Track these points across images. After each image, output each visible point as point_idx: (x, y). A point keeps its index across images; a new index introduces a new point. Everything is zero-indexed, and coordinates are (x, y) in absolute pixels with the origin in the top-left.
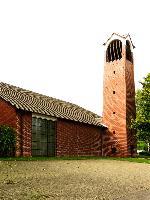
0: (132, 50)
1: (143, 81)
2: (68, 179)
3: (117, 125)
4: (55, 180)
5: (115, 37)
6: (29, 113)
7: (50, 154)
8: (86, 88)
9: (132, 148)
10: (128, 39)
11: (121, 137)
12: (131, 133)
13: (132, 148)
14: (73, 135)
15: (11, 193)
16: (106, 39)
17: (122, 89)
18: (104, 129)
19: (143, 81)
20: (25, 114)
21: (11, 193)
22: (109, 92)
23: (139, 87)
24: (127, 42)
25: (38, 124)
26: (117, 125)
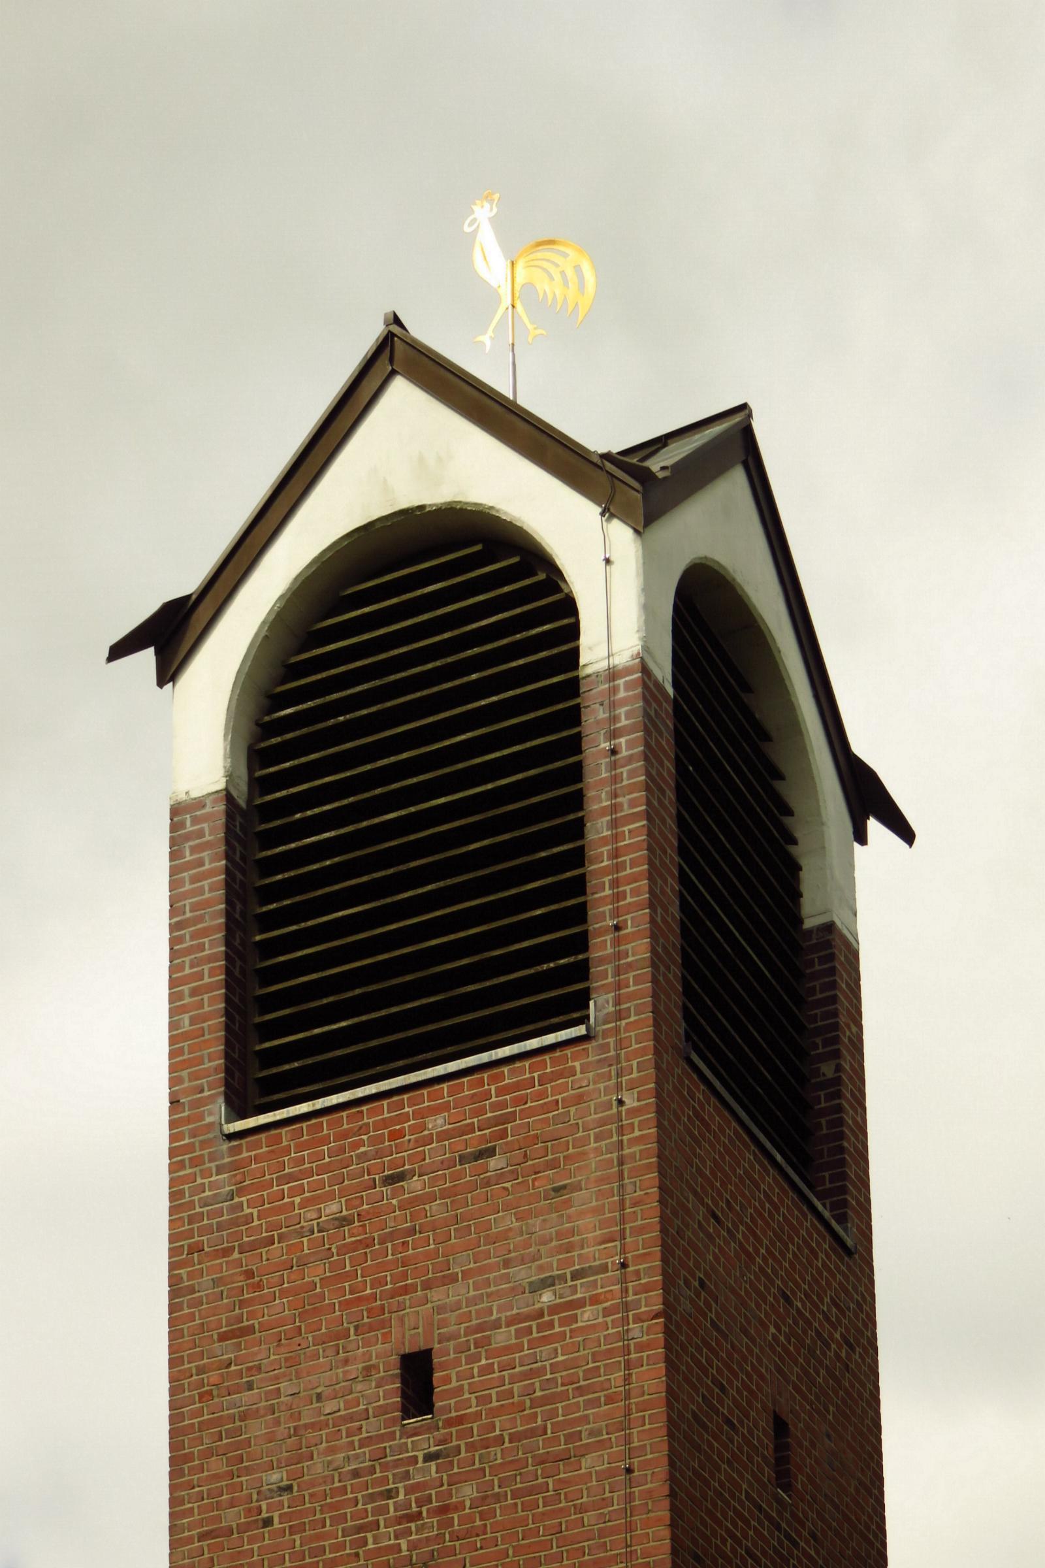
5: (416, 457)
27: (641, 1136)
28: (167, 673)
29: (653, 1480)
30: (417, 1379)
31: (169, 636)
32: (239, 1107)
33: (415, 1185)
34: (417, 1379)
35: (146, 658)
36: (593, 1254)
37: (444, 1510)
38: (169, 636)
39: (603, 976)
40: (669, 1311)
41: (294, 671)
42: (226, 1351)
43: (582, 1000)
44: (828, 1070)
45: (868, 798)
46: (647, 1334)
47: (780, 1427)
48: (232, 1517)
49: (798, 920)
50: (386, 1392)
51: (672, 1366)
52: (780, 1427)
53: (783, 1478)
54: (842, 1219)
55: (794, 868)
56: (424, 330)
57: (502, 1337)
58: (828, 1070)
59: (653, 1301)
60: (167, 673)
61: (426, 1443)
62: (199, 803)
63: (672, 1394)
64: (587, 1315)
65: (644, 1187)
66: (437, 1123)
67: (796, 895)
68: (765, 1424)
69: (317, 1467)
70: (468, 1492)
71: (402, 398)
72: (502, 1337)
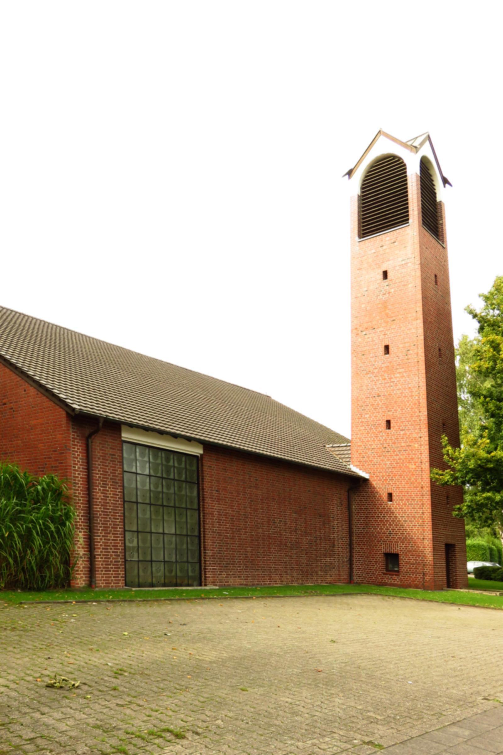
0: (442, 194)
1: (479, 306)
2: (248, 669)
3: (401, 474)
4: (198, 670)
5: (384, 148)
6: (114, 427)
7: (187, 572)
8: (298, 345)
9: (450, 551)
10: (426, 151)
11: (412, 513)
12: (444, 497)
13: (450, 551)
14: (256, 508)
15: (62, 720)
16: (356, 153)
17: (411, 334)
18: (356, 484)
19: (479, 306)
20: (95, 428)
21: (62, 720)
22: (372, 353)
23: (464, 331)
24: (425, 165)
25: (139, 467)
26: (401, 474)
27: (417, 240)
28: (350, 177)
29: (419, 288)
30: (385, 275)
31: (350, 173)
32: (360, 237)
33: (384, 247)
34: (385, 275)
35: (347, 176)
36: (410, 256)
37: (389, 293)
38: (350, 173)
39: (411, 217)
40: (421, 264)
41: (367, 176)
42: (358, 272)
43: (408, 219)
44: (441, 222)
45: (445, 181)
46: (418, 267)
47: (436, 276)
48: (359, 295)
49: (436, 201)
50: (381, 276)
51: (421, 271)
52: (436, 276)
53: (436, 282)
54: (443, 243)
55: (435, 193)
56: (385, 130)
57: (397, 268)
58: (441, 222)
59: (419, 262)
60: (350, 177)
61: (387, 284)
62: (471, 560)
63: (422, 275)
64: (410, 264)
65: (417, 246)
66: (388, 239)
67: (435, 197)
68: (434, 276)
69: (371, 288)
70: (392, 290)
71: (382, 138)
72: (397, 268)
